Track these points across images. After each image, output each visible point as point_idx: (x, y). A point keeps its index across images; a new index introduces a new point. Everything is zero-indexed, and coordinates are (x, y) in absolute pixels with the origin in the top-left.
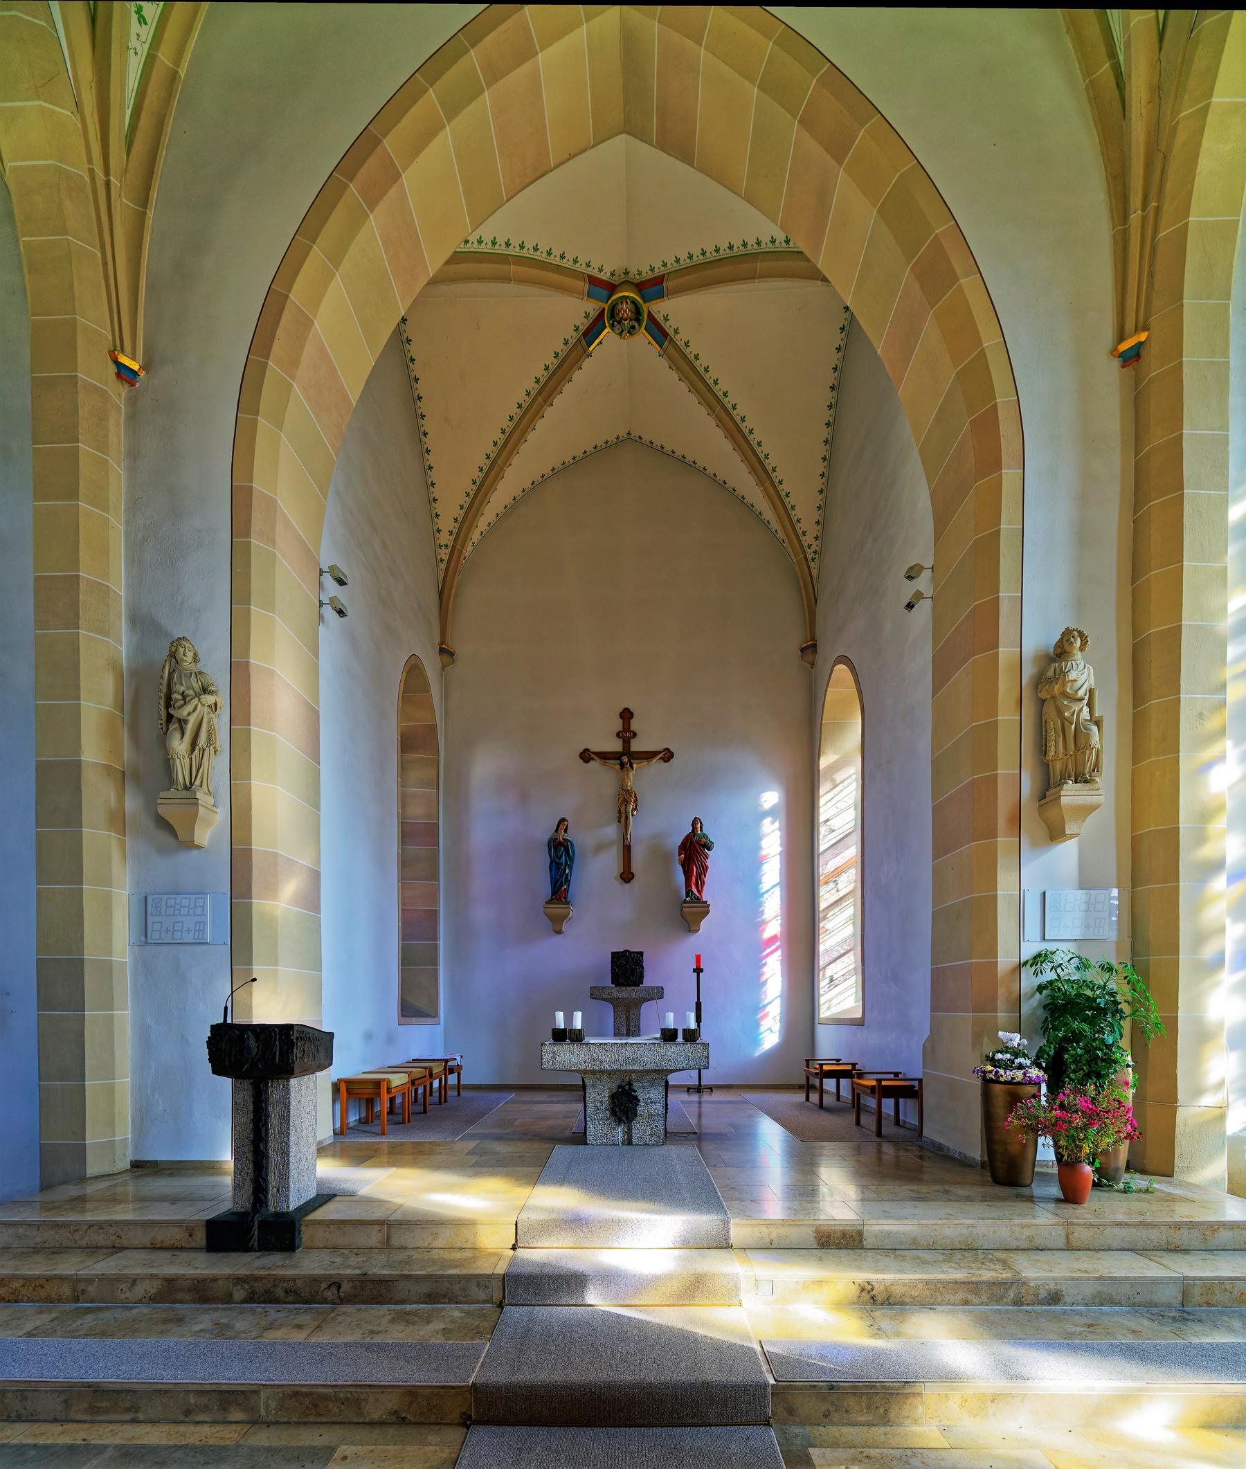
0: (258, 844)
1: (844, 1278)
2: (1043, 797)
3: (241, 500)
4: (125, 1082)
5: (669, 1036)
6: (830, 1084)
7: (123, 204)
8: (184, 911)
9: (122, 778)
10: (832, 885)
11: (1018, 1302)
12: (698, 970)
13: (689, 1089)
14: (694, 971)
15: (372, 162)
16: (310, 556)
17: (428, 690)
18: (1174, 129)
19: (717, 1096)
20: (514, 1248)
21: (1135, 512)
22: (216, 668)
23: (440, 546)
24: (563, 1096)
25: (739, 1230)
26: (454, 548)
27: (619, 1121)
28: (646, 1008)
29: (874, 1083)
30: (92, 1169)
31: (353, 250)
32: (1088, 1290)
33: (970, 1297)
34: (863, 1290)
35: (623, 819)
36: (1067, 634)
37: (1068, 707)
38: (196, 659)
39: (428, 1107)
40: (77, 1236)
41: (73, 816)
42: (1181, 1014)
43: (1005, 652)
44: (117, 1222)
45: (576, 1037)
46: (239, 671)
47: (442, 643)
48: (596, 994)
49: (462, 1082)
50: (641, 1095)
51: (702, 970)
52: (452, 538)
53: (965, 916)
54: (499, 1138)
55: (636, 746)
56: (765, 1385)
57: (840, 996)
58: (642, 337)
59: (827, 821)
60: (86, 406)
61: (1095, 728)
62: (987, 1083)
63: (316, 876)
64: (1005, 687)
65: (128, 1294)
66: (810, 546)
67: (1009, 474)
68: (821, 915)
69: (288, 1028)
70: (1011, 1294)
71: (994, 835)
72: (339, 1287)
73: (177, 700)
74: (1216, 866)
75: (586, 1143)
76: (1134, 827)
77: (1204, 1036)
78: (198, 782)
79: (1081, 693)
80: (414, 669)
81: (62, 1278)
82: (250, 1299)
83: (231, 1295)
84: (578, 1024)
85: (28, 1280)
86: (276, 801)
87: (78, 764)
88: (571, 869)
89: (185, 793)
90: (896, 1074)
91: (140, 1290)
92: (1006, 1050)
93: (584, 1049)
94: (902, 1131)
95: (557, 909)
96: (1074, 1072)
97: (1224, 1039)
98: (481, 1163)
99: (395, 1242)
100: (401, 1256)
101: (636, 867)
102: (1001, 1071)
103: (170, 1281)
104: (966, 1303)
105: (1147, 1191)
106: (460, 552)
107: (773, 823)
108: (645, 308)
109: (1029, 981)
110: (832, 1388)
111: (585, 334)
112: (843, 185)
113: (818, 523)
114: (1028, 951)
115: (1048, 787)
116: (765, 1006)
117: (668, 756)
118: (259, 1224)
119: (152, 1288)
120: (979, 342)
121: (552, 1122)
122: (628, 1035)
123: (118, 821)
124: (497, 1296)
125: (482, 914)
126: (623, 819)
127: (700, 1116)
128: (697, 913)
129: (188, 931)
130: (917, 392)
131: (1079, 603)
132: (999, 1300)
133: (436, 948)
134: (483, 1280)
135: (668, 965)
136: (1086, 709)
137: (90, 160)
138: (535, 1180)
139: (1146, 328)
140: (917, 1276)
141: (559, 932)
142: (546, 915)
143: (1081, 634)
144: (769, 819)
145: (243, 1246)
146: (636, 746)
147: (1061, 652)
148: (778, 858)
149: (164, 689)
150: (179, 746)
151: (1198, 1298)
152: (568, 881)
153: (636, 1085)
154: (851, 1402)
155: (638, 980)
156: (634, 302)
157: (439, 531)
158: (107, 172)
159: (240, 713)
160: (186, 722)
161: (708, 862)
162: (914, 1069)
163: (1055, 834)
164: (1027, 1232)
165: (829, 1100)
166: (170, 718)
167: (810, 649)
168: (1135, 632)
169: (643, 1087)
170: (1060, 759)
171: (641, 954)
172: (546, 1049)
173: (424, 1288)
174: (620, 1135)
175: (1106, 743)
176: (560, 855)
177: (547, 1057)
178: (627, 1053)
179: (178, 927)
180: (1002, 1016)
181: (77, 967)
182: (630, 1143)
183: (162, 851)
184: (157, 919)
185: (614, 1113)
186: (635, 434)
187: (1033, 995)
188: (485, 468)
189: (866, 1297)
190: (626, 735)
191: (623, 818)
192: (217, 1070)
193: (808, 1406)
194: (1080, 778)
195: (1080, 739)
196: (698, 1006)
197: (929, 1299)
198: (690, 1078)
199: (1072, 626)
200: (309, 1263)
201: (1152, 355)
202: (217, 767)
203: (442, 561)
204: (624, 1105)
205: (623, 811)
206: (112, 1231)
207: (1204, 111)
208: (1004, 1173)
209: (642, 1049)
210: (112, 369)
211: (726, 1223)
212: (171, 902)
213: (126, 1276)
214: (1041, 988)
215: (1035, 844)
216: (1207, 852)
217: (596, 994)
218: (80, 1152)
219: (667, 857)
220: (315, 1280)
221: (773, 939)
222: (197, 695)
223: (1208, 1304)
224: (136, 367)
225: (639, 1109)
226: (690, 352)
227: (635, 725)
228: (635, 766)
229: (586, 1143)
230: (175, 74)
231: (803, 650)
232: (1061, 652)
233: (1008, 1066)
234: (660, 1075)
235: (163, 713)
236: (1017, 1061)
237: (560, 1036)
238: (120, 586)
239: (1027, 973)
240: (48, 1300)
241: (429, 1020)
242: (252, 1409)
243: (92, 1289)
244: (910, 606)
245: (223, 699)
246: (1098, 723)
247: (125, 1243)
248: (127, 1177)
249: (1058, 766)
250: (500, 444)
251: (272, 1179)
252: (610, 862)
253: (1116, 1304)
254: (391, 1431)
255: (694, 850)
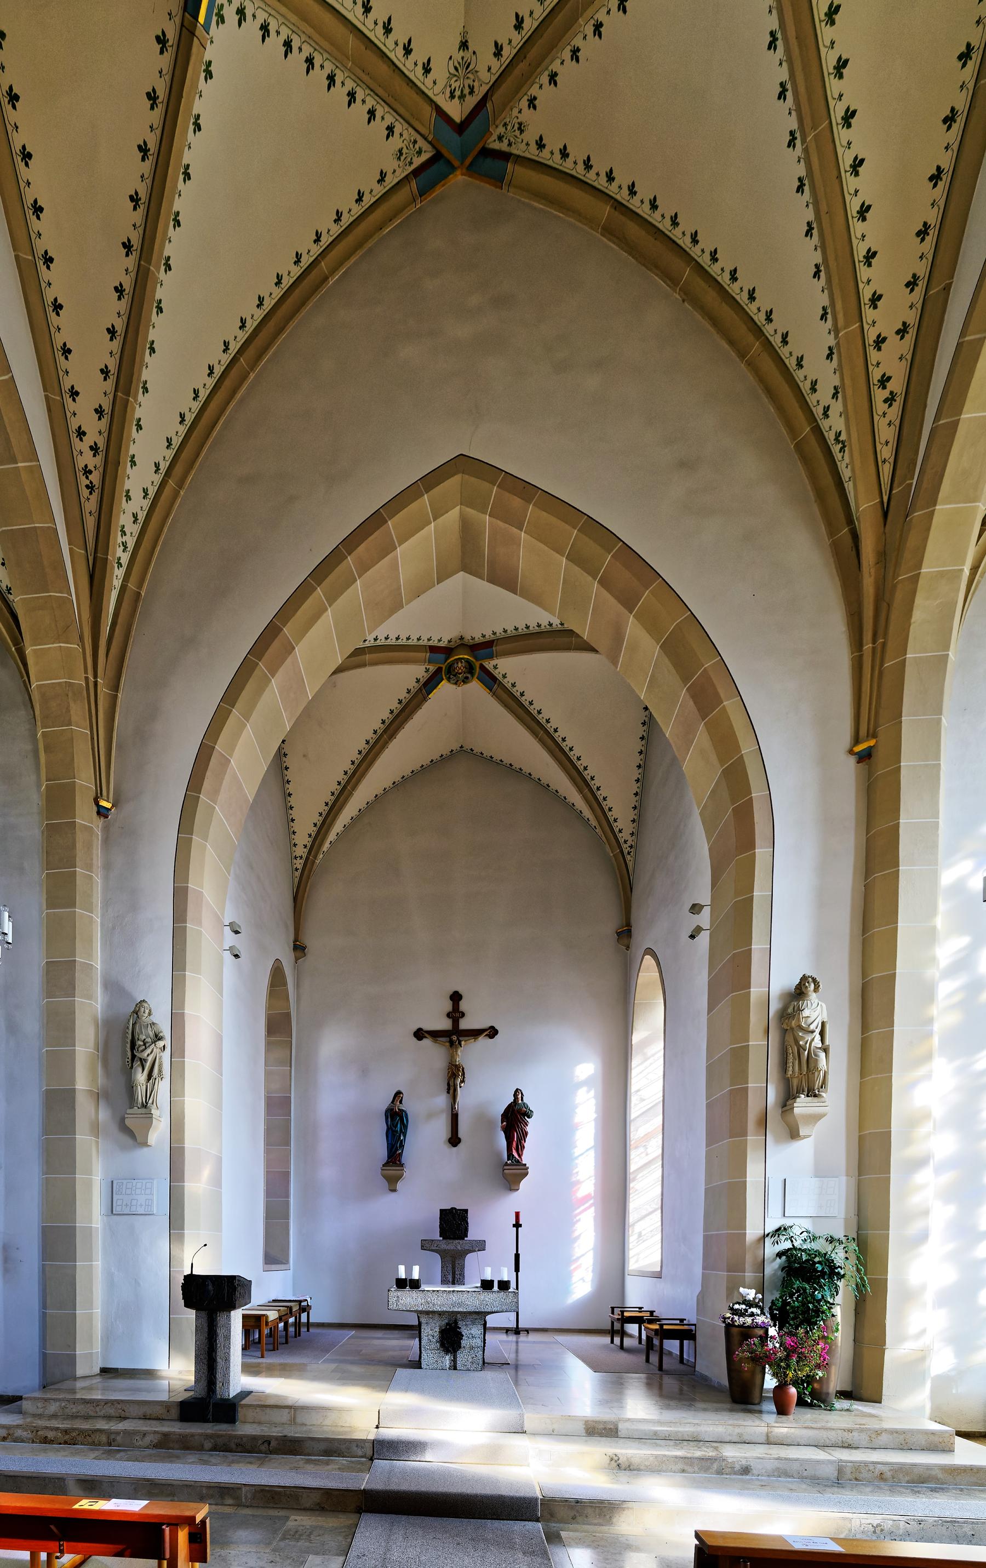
0: (188, 1144)
1: (601, 1450)
2: (784, 1105)
3: (180, 896)
4: (98, 1311)
5: (487, 1285)
6: (633, 1329)
7: (103, 691)
8: (138, 1191)
9: (99, 1096)
10: (641, 1149)
11: (720, 1472)
12: (517, 1225)
13: (507, 1330)
14: (514, 1226)
15: (276, 644)
16: (219, 920)
17: (285, 984)
18: (894, 587)
19: (532, 1337)
20: (377, 1427)
21: (866, 879)
22: (160, 1016)
23: (296, 858)
24: (396, 1333)
25: (532, 1419)
26: (307, 858)
27: (447, 1351)
28: (470, 1259)
29: (657, 1327)
30: (80, 1372)
31: (260, 706)
32: (770, 1465)
33: (686, 1468)
34: (612, 1460)
35: (451, 1091)
36: (804, 979)
37: (803, 1038)
38: (150, 1014)
39: (290, 1340)
40: (98, 1409)
41: (70, 1127)
42: (890, 1277)
43: (756, 991)
44: (122, 1401)
45: (415, 1285)
46: (177, 1020)
47: (296, 940)
48: (426, 1245)
49: (311, 1321)
50: (464, 1331)
51: (521, 1226)
52: (306, 850)
53: (726, 1197)
54: (352, 1363)
55: (464, 1024)
56: (537, 1499)
57: (645, 1251)
58: (475, 687)
59: (638, 1091)
60: (80, 837)
61: (822, 1055)
62: (729, 1327)
63: (219, 1160)
64: (755, 1021)
65: (140, 1443)
66: (625, 842)
67: (761, 852)
68: (632, 1177)
69: (232, 1278)
70: (715, 1466)
71: (744, 1133)
72: (269, 1444)
73: (140, 1046)
74: (922, 1162)
75: (420, 1368)
76: (861, 1128)
77: (909, 1296)
78: (151, 1101)
79: (812, 1027)
80: (277, 975)
81: (101, 1431)
82: (215, 1448)
83: (203, 1446)
84: (416, 1276)
85: (81, 1432)
86: (197, 1107)
87: (74, 1090)
88: (405, 1137)
89: (143, 1111)
90: (682, 1320)
91: (148, 1439)
92: (746, 1302)
93: (420, 1294)
94: (682, 1367)
95: (392, 1171)
96: (793, 1319)
97: (929, 1297)
98: (345, 1378)
99: (299, 1420)
100: (305, 1428)
101: (462, 1133)
102: (736, 1318)
103: (166, 1435)
104: (683, 1471)
105: (848, 1410)
106: (314, 862)
107: (588, 1092)
108: (477, 664)
109: (771, 1249)
110: (577, 1502)
111: (425, 684)
112: (632, 627)
113: (634, 821)
114: (770, 1228)
115: (788, 1098)
116: (578, 1258)
117: (492, 1032)
118: (209, 1406)
119: (155, 1439)
120: (738, 748)
121: (391, 1353)
122: (453, 1283)
123: (95, 1129)
124: (369, 1453)
125: (327, 1173)
126: (451, 1091)
127: (517, 1352)
128: (515, 1175)
129: (141, 1205)
130: (697, 768)
131: (819, 952)
132: (706, 1470)
133: (288, 1203)
134: (360, 1443)
135: (490, 1221)
136: (818, 1038)
137: (86, 672)
138: (386, 1389)
139: (874, 736)
140: (649, 1452)
141: (394, 1190)
142: (385, 1177)
143: (814, 980)
144: (585, 1089)
145: (204, 1419)
146: (464, 1024)
147: (799, 992)
148: (592, 1124)
149: (130, 1037)
150: (141, 1077)
151: (848, 1476)
152: (402, 1146)
153: (460, 1324)
154: (589, 1511)
155: (464, 1233)
156: (467, 661)
157: (295, 845)
158: (95, 676)
159: (178, 1050)
160: (146, 1060)
161: (528, 1129)
162: (691, 1317)
163: (794, 1134)
164: (737, 1430)
165: (627, 1342)
166: (133, 1057)
167: (625, 933)
168: (864, 974)
169: (466, 1325)
170: (799, 1078)
171: (466, 1211)
172: (391, 1294)
173: (323, 1446)
174: (448, 1362)
175: (836, 1067)
176: (396, 1121)
177: (392, 1300)
178: (454, 1298)
179: (134, 1202)
180: (749, 1275)
181: (70, 1233)
182: (455, 1368)
183: (124, 1148)
184: (121, 1197)
185: (442, 1345)
186: (467, 747)
187: (774, 1260)
188: (336, 793)
189: (614, 1464)
190: (456, 1014)
191: (452, 1090)
192: (187, 1305)
193: (562, 1512)
194: (811, 1093)
195: (811, 1063)
196: (517, 1256)
197: (657, 1468)
198: (507, 1320)
199: (808, 974)
200: (245, 1429)
201: (880, 755)
202: (163, 1088)
203: (297, 869)
204: (450, 1339)
205: (451, 1084)
206: (119, 1406)
207: (916, 579)
208: (742, 1396)
209: (465, 1296)
210: (95, 809)
211: (522, 1416)
212: (129, 1186)
213: (139, 1432)
214: (779, 1255)
215: (778, 1141)
216: (914, 1151)
217: (426, 1245)
218: (72, 1360)
219: (490, 1123)
220: (254, 1438)
221: (586, 1198)
222: (154, 1042)
223: (856, 1479)
224: (108, 805)
225: (463, 1342)
226: (516, 691)
227: (463, 1006)
228: (463, 1043)
229: (420, 1368)
230: (139, 594)
231: (619, 934)
232: (799, 992)
233: (741, 1314)
234: (480, 1316)
235: (129, 1054)
236: (750, 1311)
237: (401, 1284)
238: (98, 965)
239: (768, 1241)
240: (93, 1444)
241: (282, 1267)
242: (237, 1498)
243: (119, 1438)
244: (692, 937)
245: (167, 1042)
246: (826, 1050)
247: (127, 1415)
248: (98, 1379)
249: (795, 1082)
250: (349, 773)
251: (219, 1376)
252: (441, 1128)
253: (790, 1477)
254: (317, 1513)
255: (515, 1118)
